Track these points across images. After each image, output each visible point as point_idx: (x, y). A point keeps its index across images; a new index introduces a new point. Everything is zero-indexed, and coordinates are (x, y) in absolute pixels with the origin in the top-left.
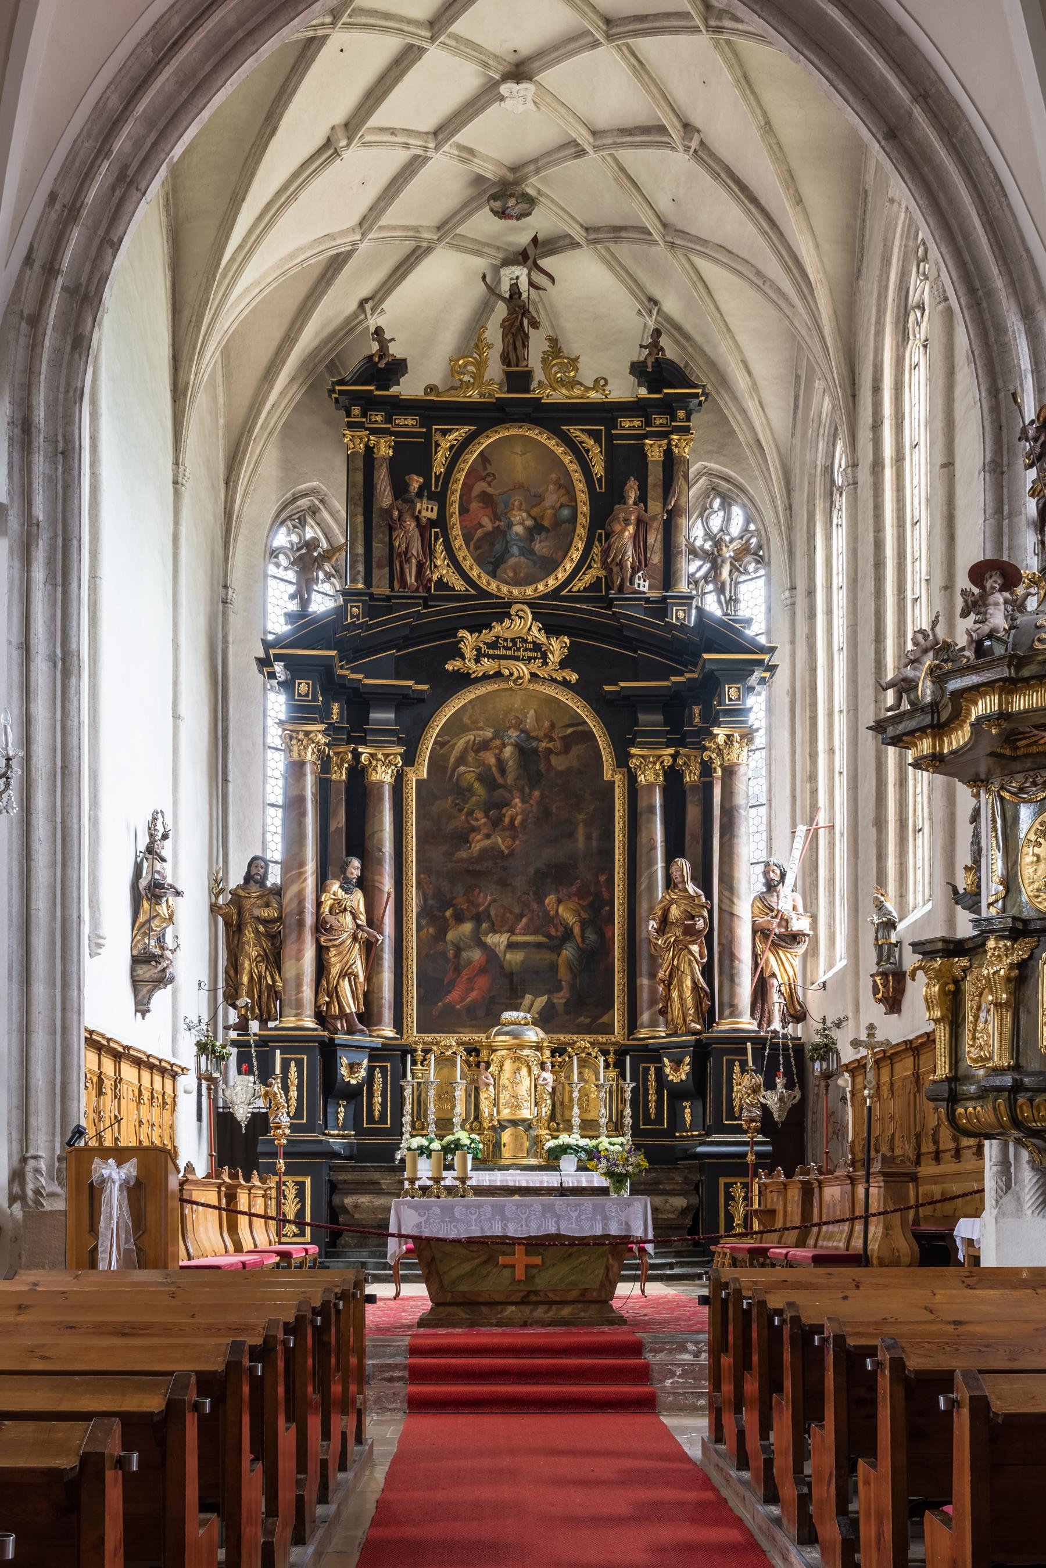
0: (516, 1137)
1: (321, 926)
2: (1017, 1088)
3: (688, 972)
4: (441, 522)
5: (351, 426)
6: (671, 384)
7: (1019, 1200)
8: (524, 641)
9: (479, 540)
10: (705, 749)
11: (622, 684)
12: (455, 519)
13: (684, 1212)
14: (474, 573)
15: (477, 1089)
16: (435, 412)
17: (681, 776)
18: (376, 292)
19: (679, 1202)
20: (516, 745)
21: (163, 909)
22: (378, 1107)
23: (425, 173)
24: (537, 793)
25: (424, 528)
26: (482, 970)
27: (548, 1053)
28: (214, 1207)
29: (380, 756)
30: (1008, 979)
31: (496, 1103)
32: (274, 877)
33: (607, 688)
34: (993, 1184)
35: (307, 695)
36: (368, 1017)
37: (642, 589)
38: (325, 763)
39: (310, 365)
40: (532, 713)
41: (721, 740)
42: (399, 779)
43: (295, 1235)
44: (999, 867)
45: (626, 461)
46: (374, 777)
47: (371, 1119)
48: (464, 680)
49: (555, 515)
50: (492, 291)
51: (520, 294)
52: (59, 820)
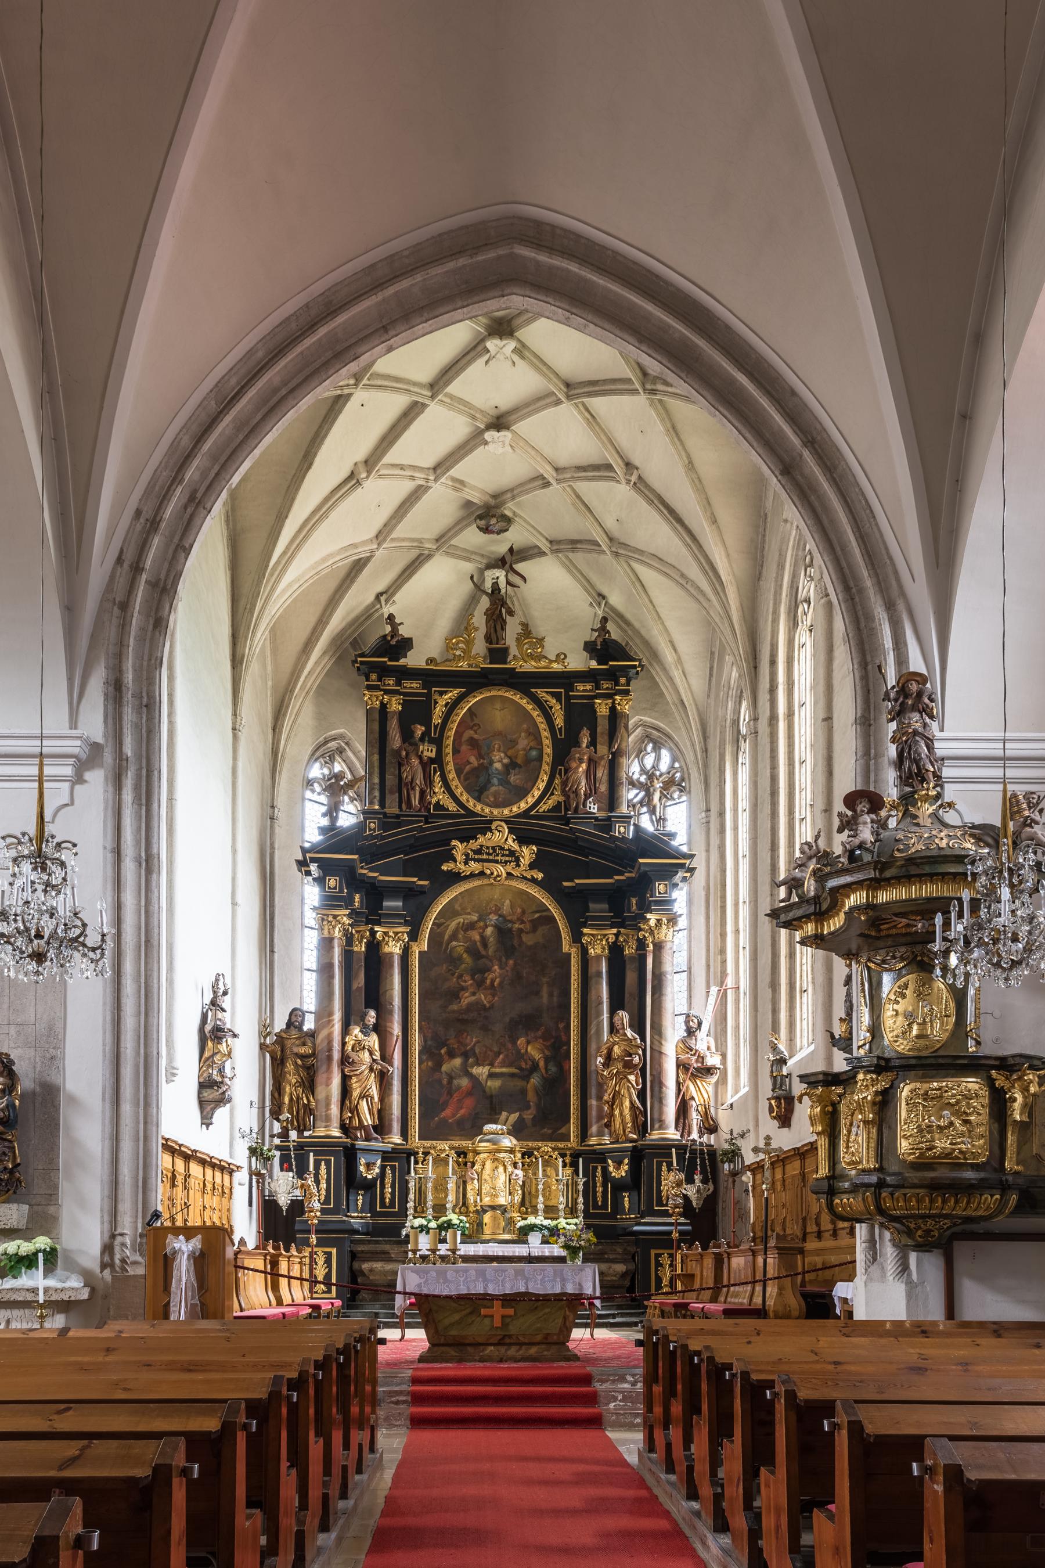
0: (494, 1219)
3: (627, 1095)
5: (369, 688)
6: (615, 658)
9: (468, 773)
10: (640, 929)
11: (577, 881)
12: (449, 758)
13: (624, 1275)
14: (464, 798)
15: (465, 1183)
16: (434, 678)
17: (621, 949)
18: (389, 588)
19: (620, 1268)
20: (496, 926)
21: (223, 1047)
24: (511, 962)
25: (426, 764)
26: (469, 1093)
27: (519, 1155)
28: (261, 1272)
29: (391, 934)
30: (874, 1103)
31: (479, 1193)
32: (309, 1024)
33: (565, 884)
35: (335, 888)
36: (381, 1128)
38: (349, 939)
39: (337, 641)
41: (652, 923)
43: (324, 1292)
44: (866, 1019)
45: (580, 716)
46: (387, 949)
48: (456, 877)
49: (526, 755)
50: (478, 587)
51: (500, 590)
52: (143, 981)
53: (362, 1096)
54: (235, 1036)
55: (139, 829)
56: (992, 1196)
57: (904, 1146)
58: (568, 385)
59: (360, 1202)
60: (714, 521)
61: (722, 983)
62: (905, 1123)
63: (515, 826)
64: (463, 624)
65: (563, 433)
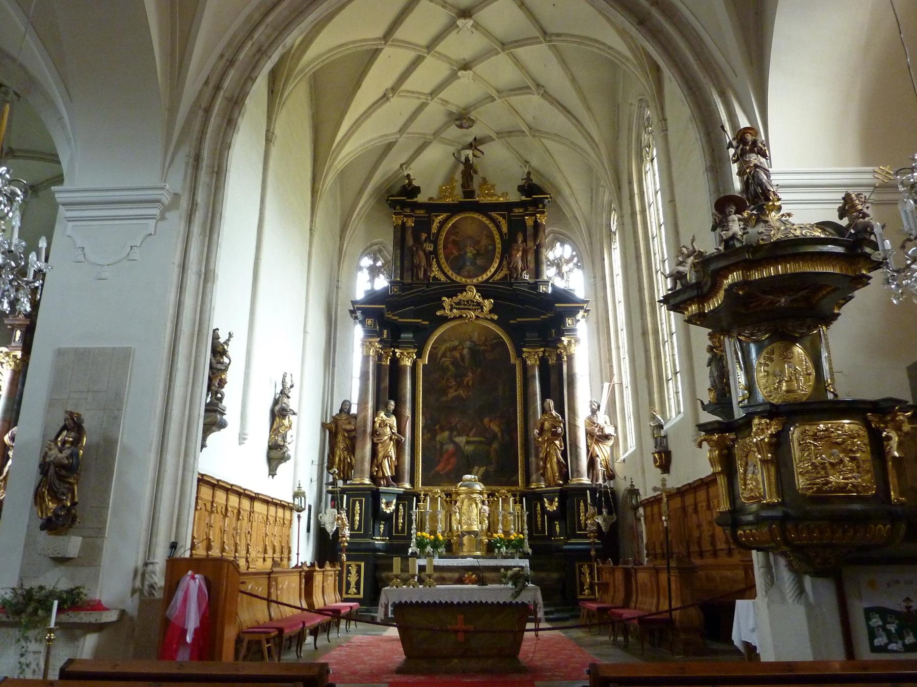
0: (470, 540)
1: (374, 433)
2: (785, 518)
4: (435, 252)
5: (395, 214)
6: (534, 194)
7: (781, 591)
10: (558, 348)
12: (441, 251)
14: (450, 273)
15: (450, 515)
16: (433, 208)
17: (547, 361)
19: (555, 575)
20: (470, 348)
21: (286, 422)
23: (427, 109)
24: (479, 370)
25: (428, 255)
26: (453, 454)
27: (486, 496)
28: (264, 599)
30: (770, 444)
31: (460, 522)
32: (354, 410)
34: (762, 580)
36: (397, 478)
38: (380, 357)
39: (377, 190)
41: (565, 343)
42: (414, 364)
44: (742, 379)
45: (517, 226)
46: (402, 363)
48: (445, 319)
50: (458, 160)
52: (193, 359)
53: (384, 457)
54: (294, 414)
55: (202, 253)
56: (885, 526)
57: (801, 482)
58: (503, 44)
60: (589, 109)
62: (800, 461)
63: (479, 288)
64: (449, 179)
65: (501, 71)
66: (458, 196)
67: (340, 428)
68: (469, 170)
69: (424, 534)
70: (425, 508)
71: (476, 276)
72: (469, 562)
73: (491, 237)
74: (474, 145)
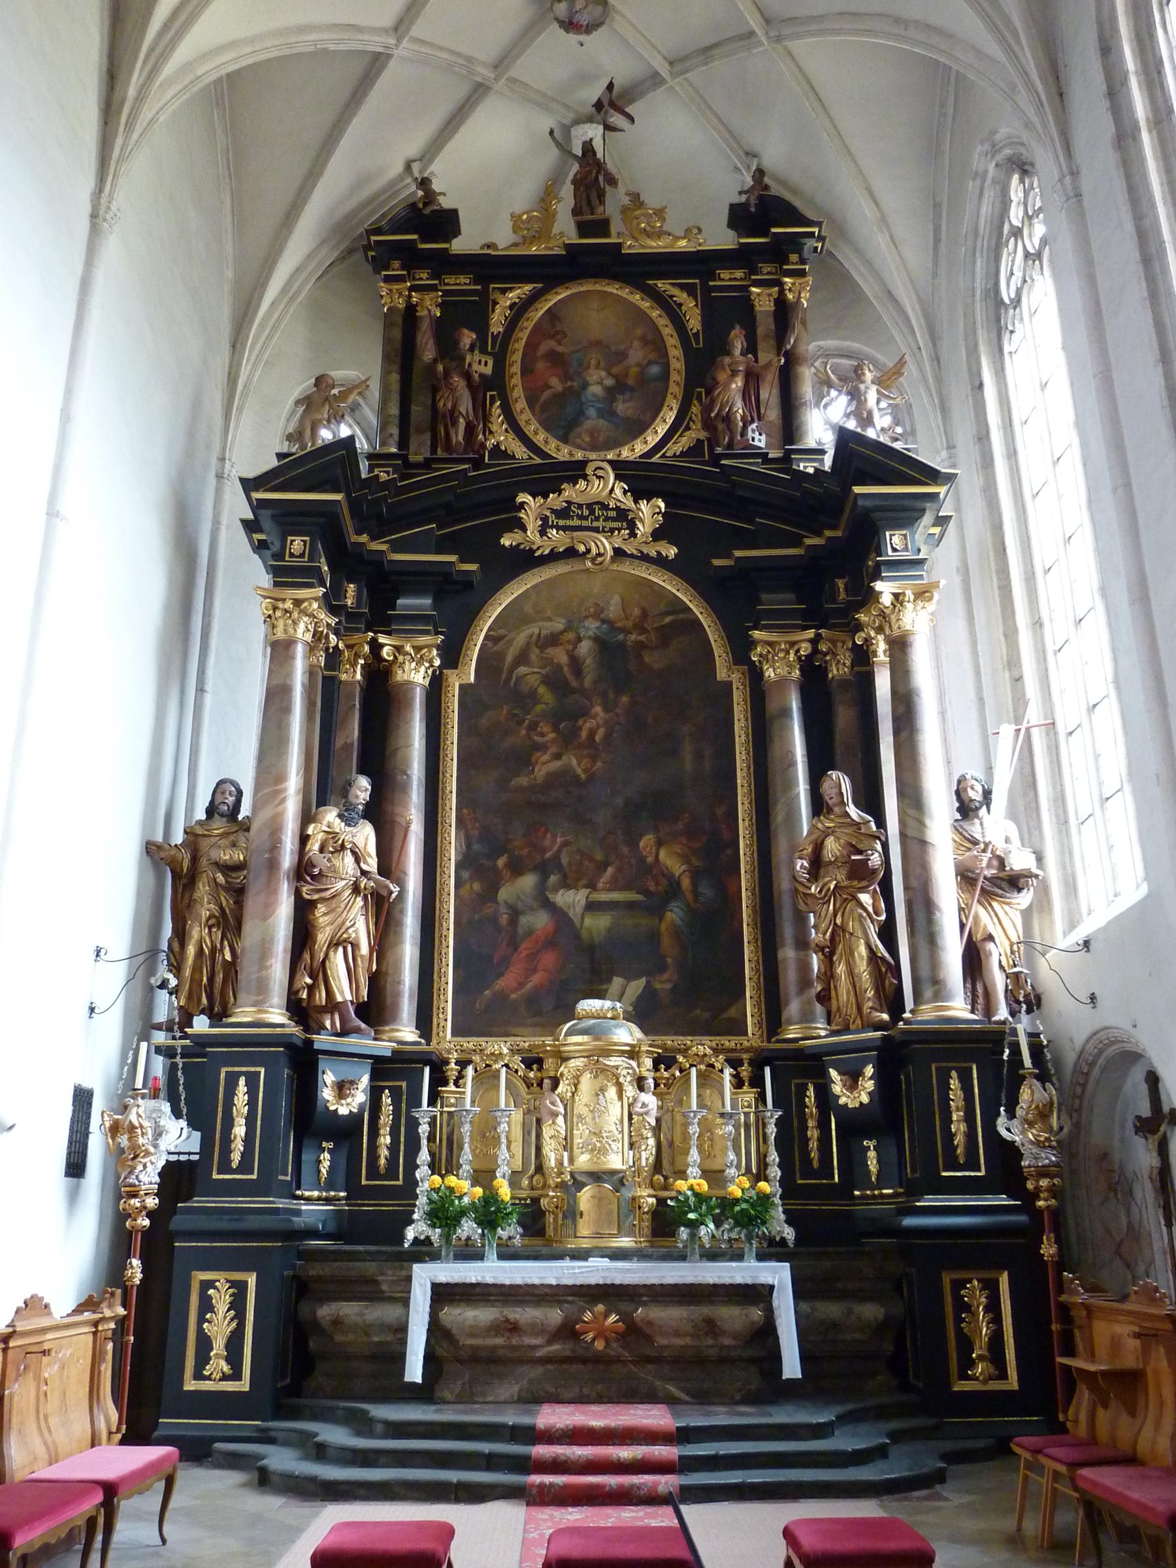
0: (599, 1200)
1: (303, 870)
3: (860, 933)
4: (496, 383)
5: (387, 279)
6: (772, 224)
8: (605, 507)
10: (859, 627)
11: (738, 553)
13: (881, 1328)
14: (540, 438)
15: (539, 1121)
16: (493, 268)
17: (823, 670)
19: (871, 1312)
20: (596, 639)
22: (384, 1153)
26: (551, 943)
27: (648, 1062)
29: (408, 648)
31: (567, 1144)
33: (717, 562)
35: (302, 555)
36: (374, 1010)
37: (756, 443)
39: (339, 228)
40: (616, 599)
41: (886, 600)
42: (436, 687)
43: (225, 1378)
47: (373, 1172)
48: (526, 560)
49: (641, 373)
51: (594, 153)
53: (335, 944)
59: (325, 1165)
61: (1018, 720)
66: (565, 229)
67: (204, 862)
68: (592, 178)
69: (452, 1180)
70: (460, 1100)
71: (617, 444)
72: (596, 1271)
73: (656, 343)
74: (612, 104)
